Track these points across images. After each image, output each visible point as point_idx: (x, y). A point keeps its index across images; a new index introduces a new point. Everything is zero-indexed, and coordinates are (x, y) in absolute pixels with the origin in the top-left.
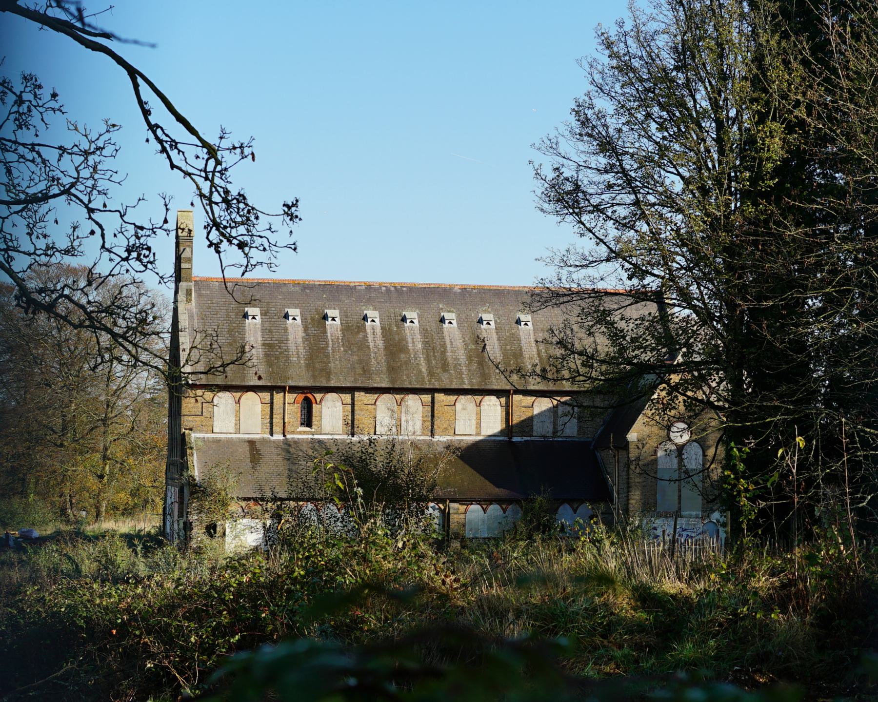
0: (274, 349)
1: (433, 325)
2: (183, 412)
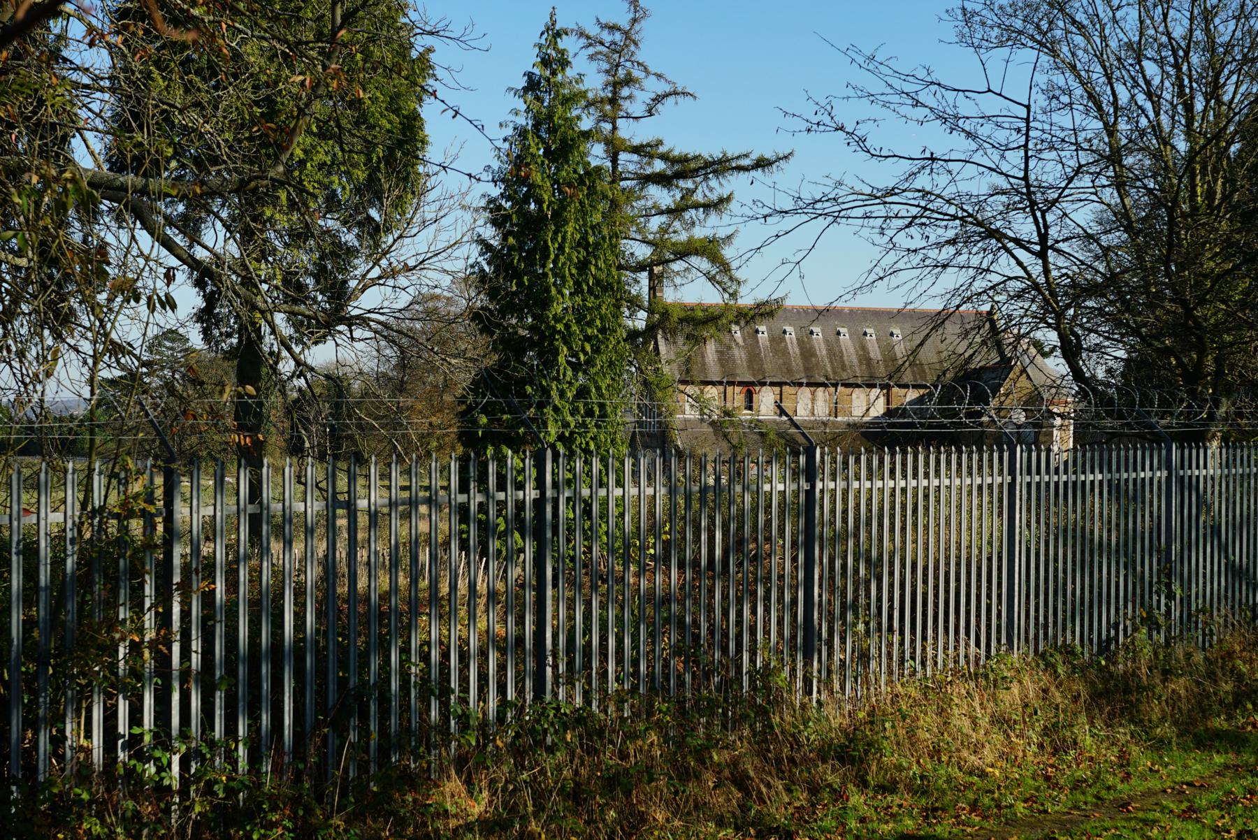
1: (832, 337)
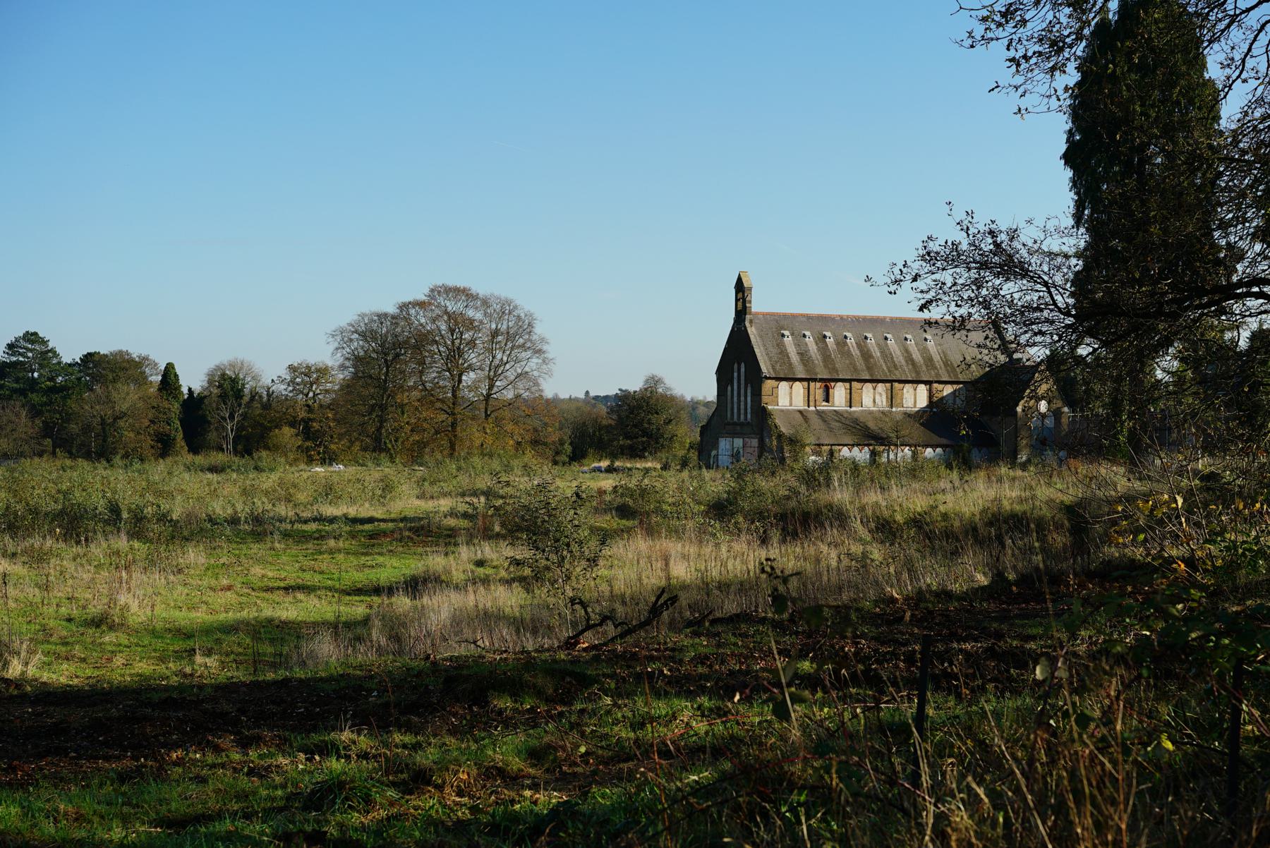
0: (803, 355)
1: (882, 341)
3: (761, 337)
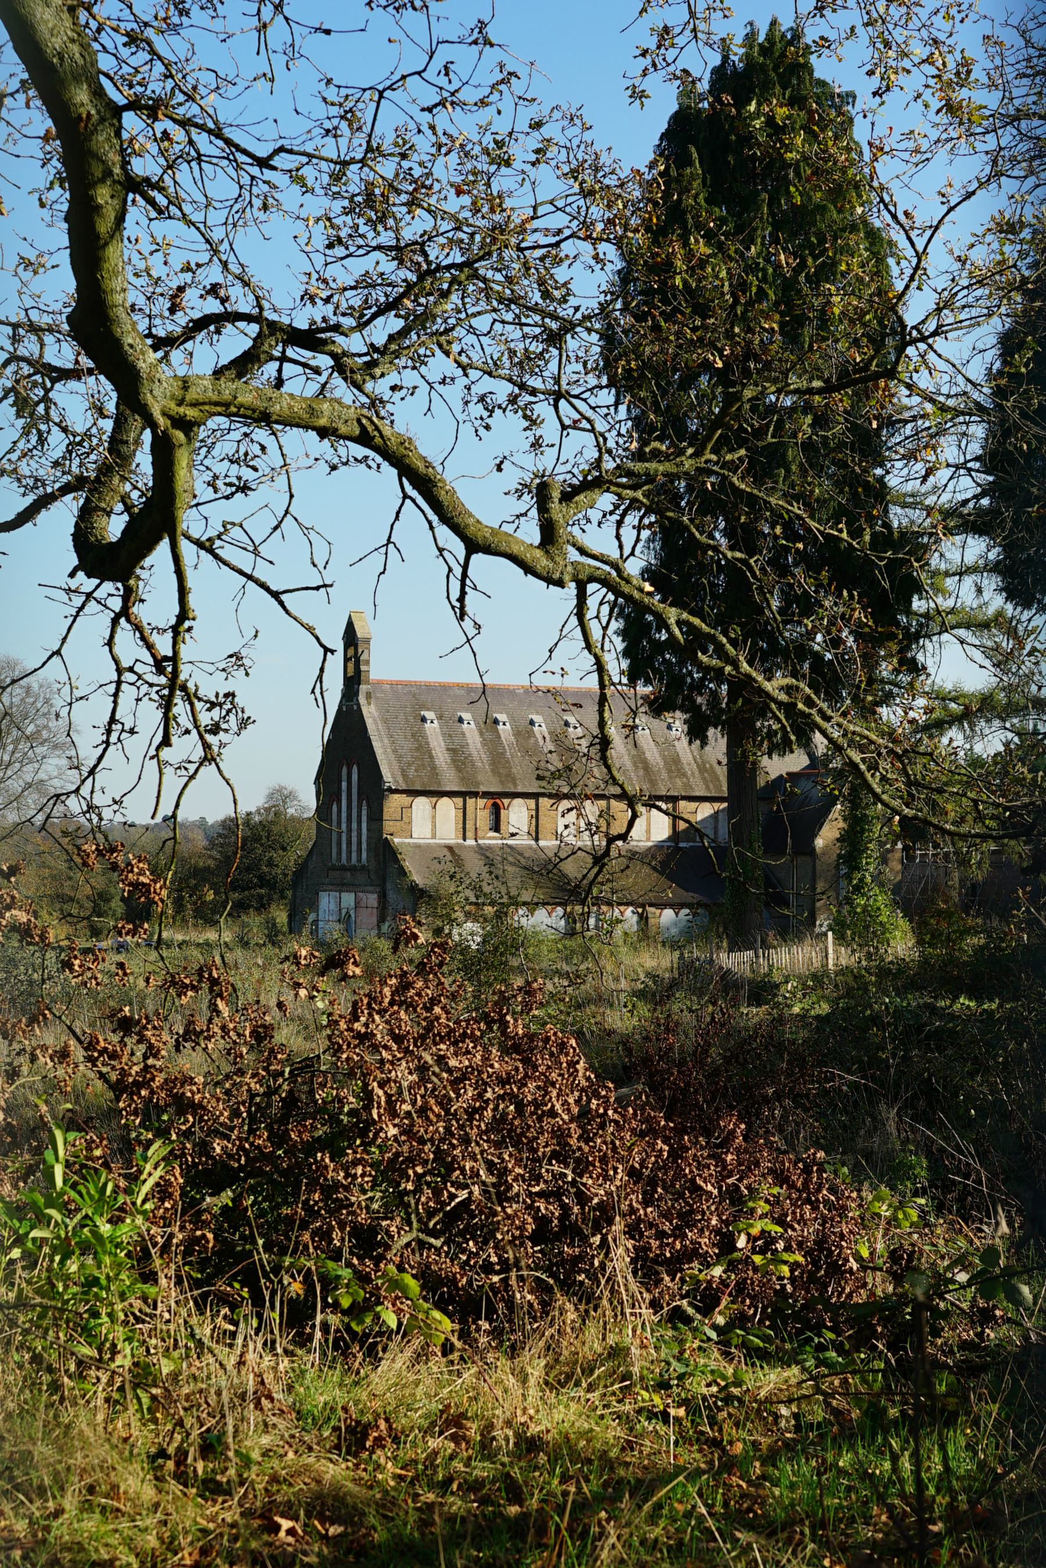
0: (458, 754)
2: (386, 816)
3: (385, 721)
